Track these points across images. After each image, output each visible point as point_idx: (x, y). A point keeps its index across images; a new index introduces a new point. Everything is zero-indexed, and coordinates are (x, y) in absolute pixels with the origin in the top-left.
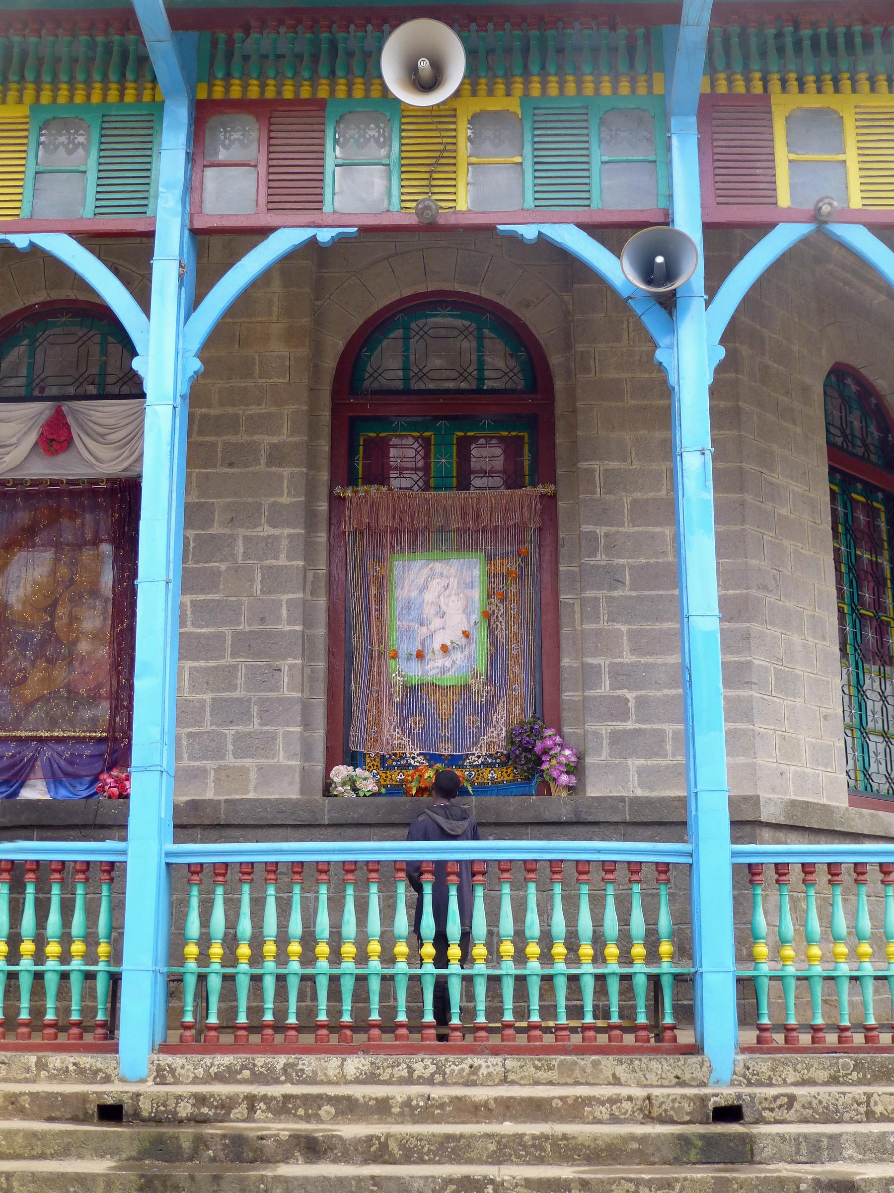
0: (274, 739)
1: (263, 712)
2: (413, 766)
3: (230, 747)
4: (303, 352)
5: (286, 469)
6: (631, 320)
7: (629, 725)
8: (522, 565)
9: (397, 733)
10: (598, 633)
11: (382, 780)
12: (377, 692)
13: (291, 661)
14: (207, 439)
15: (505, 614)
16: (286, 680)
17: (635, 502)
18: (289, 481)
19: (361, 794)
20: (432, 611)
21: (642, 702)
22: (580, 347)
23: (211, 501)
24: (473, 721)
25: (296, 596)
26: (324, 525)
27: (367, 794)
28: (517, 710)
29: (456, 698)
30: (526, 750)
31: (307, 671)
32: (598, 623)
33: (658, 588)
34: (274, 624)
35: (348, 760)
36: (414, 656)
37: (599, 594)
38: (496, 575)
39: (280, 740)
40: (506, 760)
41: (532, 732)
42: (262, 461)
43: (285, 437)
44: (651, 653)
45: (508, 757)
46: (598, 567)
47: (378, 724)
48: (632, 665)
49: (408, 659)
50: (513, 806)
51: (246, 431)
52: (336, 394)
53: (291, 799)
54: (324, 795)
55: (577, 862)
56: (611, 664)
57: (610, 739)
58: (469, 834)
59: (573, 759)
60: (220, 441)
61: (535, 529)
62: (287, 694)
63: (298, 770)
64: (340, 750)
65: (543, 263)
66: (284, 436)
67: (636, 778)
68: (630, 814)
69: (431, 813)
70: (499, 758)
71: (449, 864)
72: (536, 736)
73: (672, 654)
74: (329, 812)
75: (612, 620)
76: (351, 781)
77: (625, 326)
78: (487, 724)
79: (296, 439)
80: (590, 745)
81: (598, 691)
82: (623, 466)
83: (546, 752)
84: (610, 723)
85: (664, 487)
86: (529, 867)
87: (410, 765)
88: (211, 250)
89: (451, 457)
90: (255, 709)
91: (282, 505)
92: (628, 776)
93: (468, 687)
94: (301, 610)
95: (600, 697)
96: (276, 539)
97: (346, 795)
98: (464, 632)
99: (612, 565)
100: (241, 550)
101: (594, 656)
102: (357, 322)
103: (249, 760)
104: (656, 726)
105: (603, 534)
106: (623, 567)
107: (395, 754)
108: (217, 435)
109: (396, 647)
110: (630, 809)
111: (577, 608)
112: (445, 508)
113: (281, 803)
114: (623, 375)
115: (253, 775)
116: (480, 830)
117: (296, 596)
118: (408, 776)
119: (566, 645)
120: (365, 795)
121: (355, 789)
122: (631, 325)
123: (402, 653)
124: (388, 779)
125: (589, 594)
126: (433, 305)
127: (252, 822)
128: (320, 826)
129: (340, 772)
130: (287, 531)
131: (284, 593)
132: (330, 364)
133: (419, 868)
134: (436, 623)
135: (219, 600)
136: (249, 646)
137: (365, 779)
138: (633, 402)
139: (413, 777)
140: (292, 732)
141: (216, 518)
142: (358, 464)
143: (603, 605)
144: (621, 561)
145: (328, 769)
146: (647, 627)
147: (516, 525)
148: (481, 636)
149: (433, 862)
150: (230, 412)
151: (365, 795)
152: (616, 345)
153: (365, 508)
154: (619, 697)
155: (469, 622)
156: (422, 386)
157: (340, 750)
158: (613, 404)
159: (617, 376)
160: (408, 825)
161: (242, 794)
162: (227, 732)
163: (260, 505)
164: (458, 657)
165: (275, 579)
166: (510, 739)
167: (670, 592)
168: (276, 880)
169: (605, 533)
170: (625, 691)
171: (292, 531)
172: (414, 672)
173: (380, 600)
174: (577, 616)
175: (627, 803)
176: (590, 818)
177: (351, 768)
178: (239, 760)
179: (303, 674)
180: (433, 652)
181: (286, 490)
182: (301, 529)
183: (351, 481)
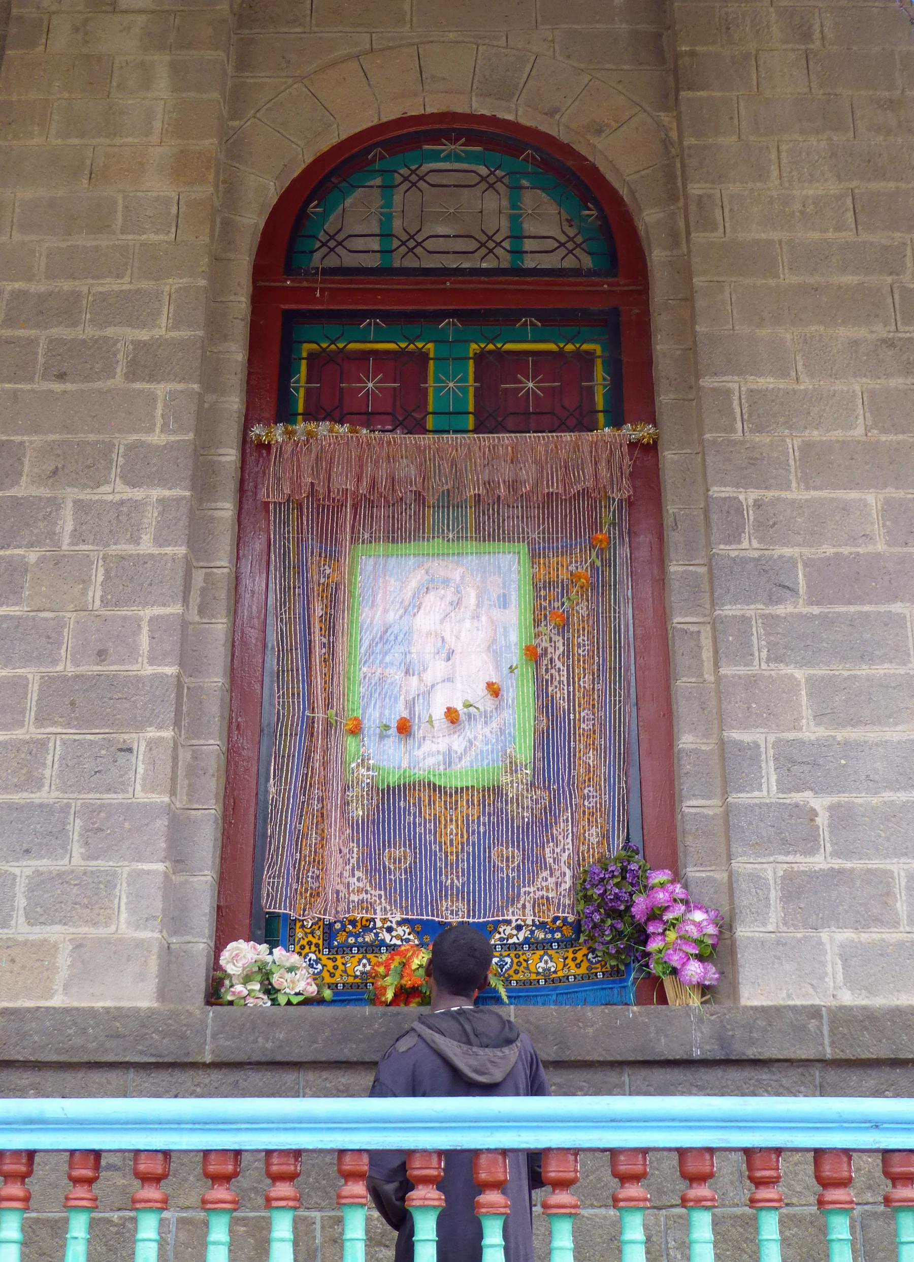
0: (111, 885)
1: (91, 832)
2: (388, 946)
3: (21, 901)
4: (204, 191)
5: (162, 386)
6: (784, 147)
7: (819, 862)
8: (598, 563)
9: (358, 880)
10: (752, 682)
11: (326, 974)
12: (321, 800)
13: (152, 733)
14: (21, 333)
15: (567, 654)
16: (141, 770)
17: (807, 447)
18: (165, 406)
19: (282, 1000)
20: (429, 649)
21: (843, 818)
22: (695, 189)
23: (18, 438)
24: (506, 857)
25: (168, 610)
26: (229, 486)
27: (295, 1000)
28: (593, 835)
29: (474, 812)
30: (614, 913)
31: (185, 755)
32: (750, 663)
33: (860, 600)
34: (122, 661)
35: (260, 933)
36: (393, 731)
37: (751, 610)
38: (549, 584)
39: (122, 890)
40: (574, 934)
41: (624, 878)
42: (118, 370)
43: (163, 332)
44: (854, 722)
45: (577, 927)
46: (745, 561)
47: (319, 862)
48: (819, 744)
49: (382, 737)
50: (597, 1024)
51: (91, 320)
52: (259, 272)
53: (137, 1010)
54: (208, 1003)
55: (819, 1153)
56: (777, 743)
57: (782, 889)
58: (522, 1080)
59: (711, 930)
60: (43, 336)
61: (621, 501)
62: (142, 796)
63: (155, 949)
64: (247, 913)
65: (625, 67)
66: (161, 329)
67: (839, 967)
68: (832, 1044)
69: (427, 1032)
70: (559, 929)
71: (483, 1160)
72: (632, 885)
73: (896, 724)
74: (214, 1036)
75: (776, 658)
76: (263, 974)
77: (774, 156)
78: (534, 864)
79: (184, 334)
80: (743, 901)
81: (756, 794)
82: (782, 384)
83: (655, 915)
84: (781, 858)
85: (861, 420)
86: (693, 1167)
87: (383, 943)
88: (50, 35)
89: (464, 379)
90: (76, 827)
91: (149, 446)
92: (823, 964)
93: (497, 791)
94: (177, 637)
95: (760, 806)
96: (137, 506)
97: (251, 1002)
98: (490, 685)
99: (771, 557)
100: (69, 526)
101: (744, 726)
102: (301, 155)
103: (58, 928)
104: (875, 864)
105: (751, 502)
106: (793, 562)
107: (353, 922)
108: (37, 326)
109: (359, 714)
110: (832, 1032)
111: (706, 642)
112: (454, 463)
113: (115, 1018)
114: (775, 235)
115: (64, 960)
116: (545, 1075)
117: (168, 610)
118: (379, 964)
119: (684, 709)
120: (289, 1003)
121: (270, 991)
122: (784, 155)
123: (371, 722)
124: (338, 973)
125: (730, 610)
126: (435, 137)
127: (54, 1058)
128: (194, 1065)
129: (242, 955)
130: (157, 493)
131: (145, 605)
132: (252, 219)
133: (403, 1167)
134: (437, 669)
135: (20, 618)
136: (72, 704)
137: (291, 969)
138: (794, 279)
139: (388, 968)
140: (148, 872)
141: (26, 469)
142: (297, 389)
143: (757, 631)
144: (787, 551)
145: (218, 949)
146: (843, 671)
147: (585, 493)
148: (521, 695)
149: (440, 1153)
150: (66, 288)
151: (289, 1003)
152: (759, 185)
153: (307, 461)
154: (797, 806)
155: (497, 666)
156: (410, 262)
157: (247, 913)
158: (760, 281)
159: (763, 236)
160: (372, 1065)
161: (41, 997)
162: (17, 871)
163: (110, 447)
164: (480, 733)
165: (128, 580)
166: (582, 892)
167: (882, 608)
168: (26, 1199)
169: (755, 501)
170: (808, 794)
171: (167, 493)
172: (391, 760)
173: (330, 626)
174: (707, 655)
175: (825, 1020)
176: (752, 1052)
177: (264, 947)
178: (37, 929)
179: (175, 759)
180: (430, 721)
181: (159, 421)
182: (185, 489)
183: (284, 413)
